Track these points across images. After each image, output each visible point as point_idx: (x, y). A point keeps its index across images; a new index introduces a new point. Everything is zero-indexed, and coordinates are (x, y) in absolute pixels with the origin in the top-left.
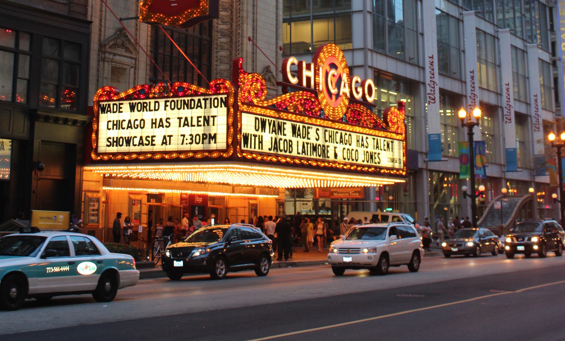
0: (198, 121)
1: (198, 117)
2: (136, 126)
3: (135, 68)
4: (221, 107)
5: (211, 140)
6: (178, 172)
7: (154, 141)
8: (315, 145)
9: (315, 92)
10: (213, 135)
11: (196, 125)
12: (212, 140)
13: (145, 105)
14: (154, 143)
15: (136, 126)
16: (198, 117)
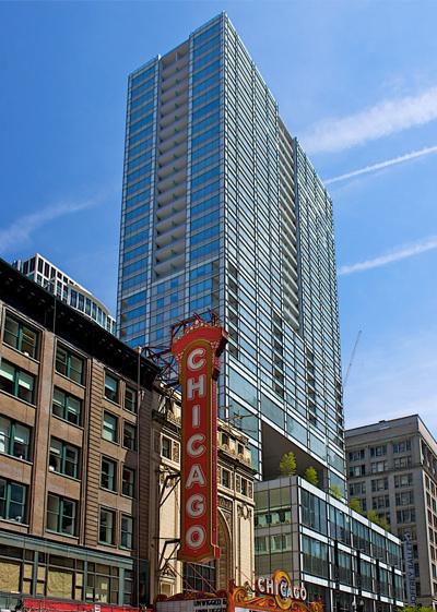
3: (175, 584)
9: (274, 596)
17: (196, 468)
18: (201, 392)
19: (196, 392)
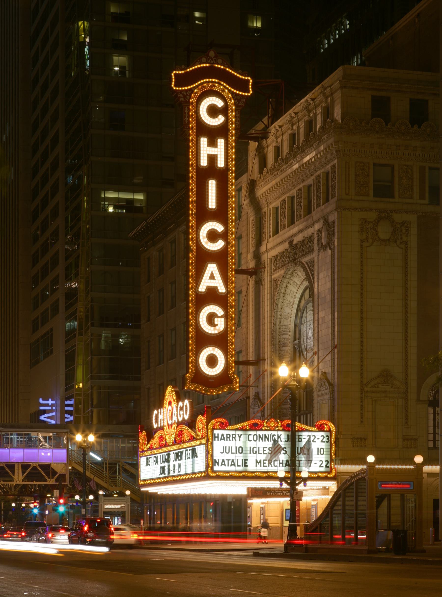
0: (264, 451)
1: (264, 448)
2: (254, 452)
4: (259, 441)
5: (257, 464)
6: (228, 485)
7: (247, 463)
8: (270, 465)
10: (259, 461)
11: (262, 453)
12: (258, 464)
13: (234, 436)
14: (247, 464)
15: (254, 452)
16: (264, 448)
18: (221, 163)
19: (212, 159)
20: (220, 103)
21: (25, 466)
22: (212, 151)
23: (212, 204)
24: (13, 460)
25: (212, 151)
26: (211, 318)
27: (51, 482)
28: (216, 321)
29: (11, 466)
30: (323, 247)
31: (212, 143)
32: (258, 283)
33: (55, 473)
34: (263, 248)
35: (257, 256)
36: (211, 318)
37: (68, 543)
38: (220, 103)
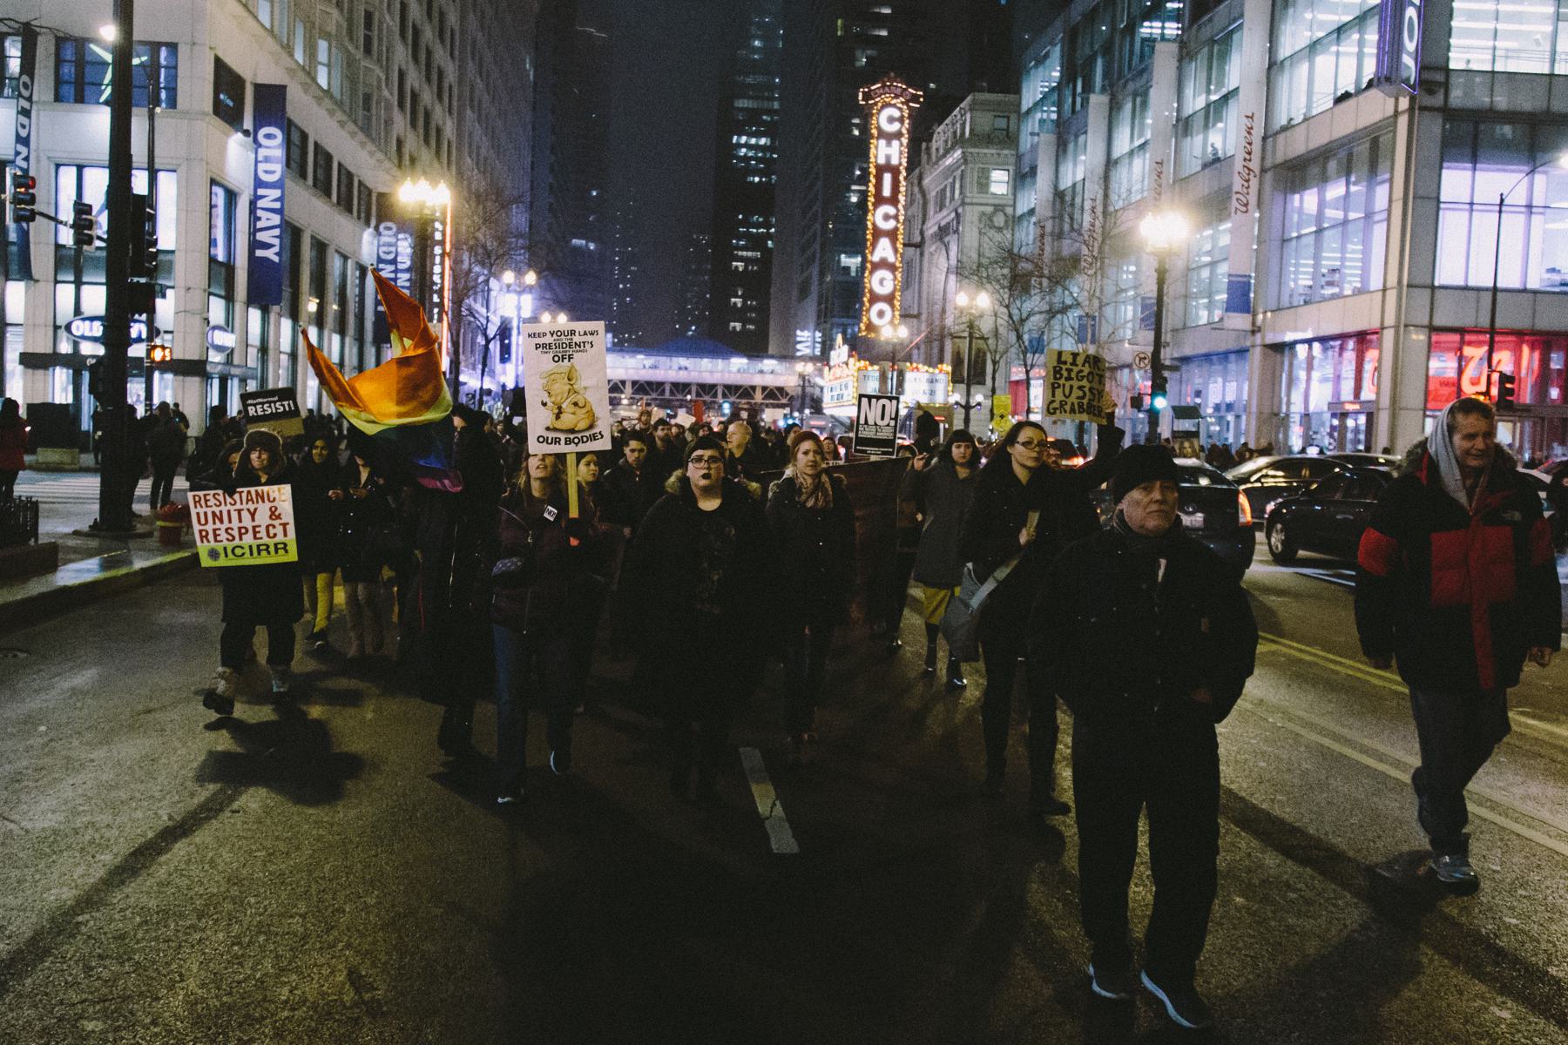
13: (204, 533)
17: (884, 243)
19: (888, 157)
20: (897, 114)
21: (764, 388)
22: (889, 151)
23: (887, 192)
24: (754, 384)
25: (889, 151)
26: (881, 282)
27: (784, 401)
28: (885, 283)
29: (754, 388)
30: (954, 232)
31: (889, 144)
32: (922, 254)
33: (787, 394)
34: (925, 227)
35: (922, 233)
36: (881, 282)
37: (1175, 429)
38: (897, 114)
